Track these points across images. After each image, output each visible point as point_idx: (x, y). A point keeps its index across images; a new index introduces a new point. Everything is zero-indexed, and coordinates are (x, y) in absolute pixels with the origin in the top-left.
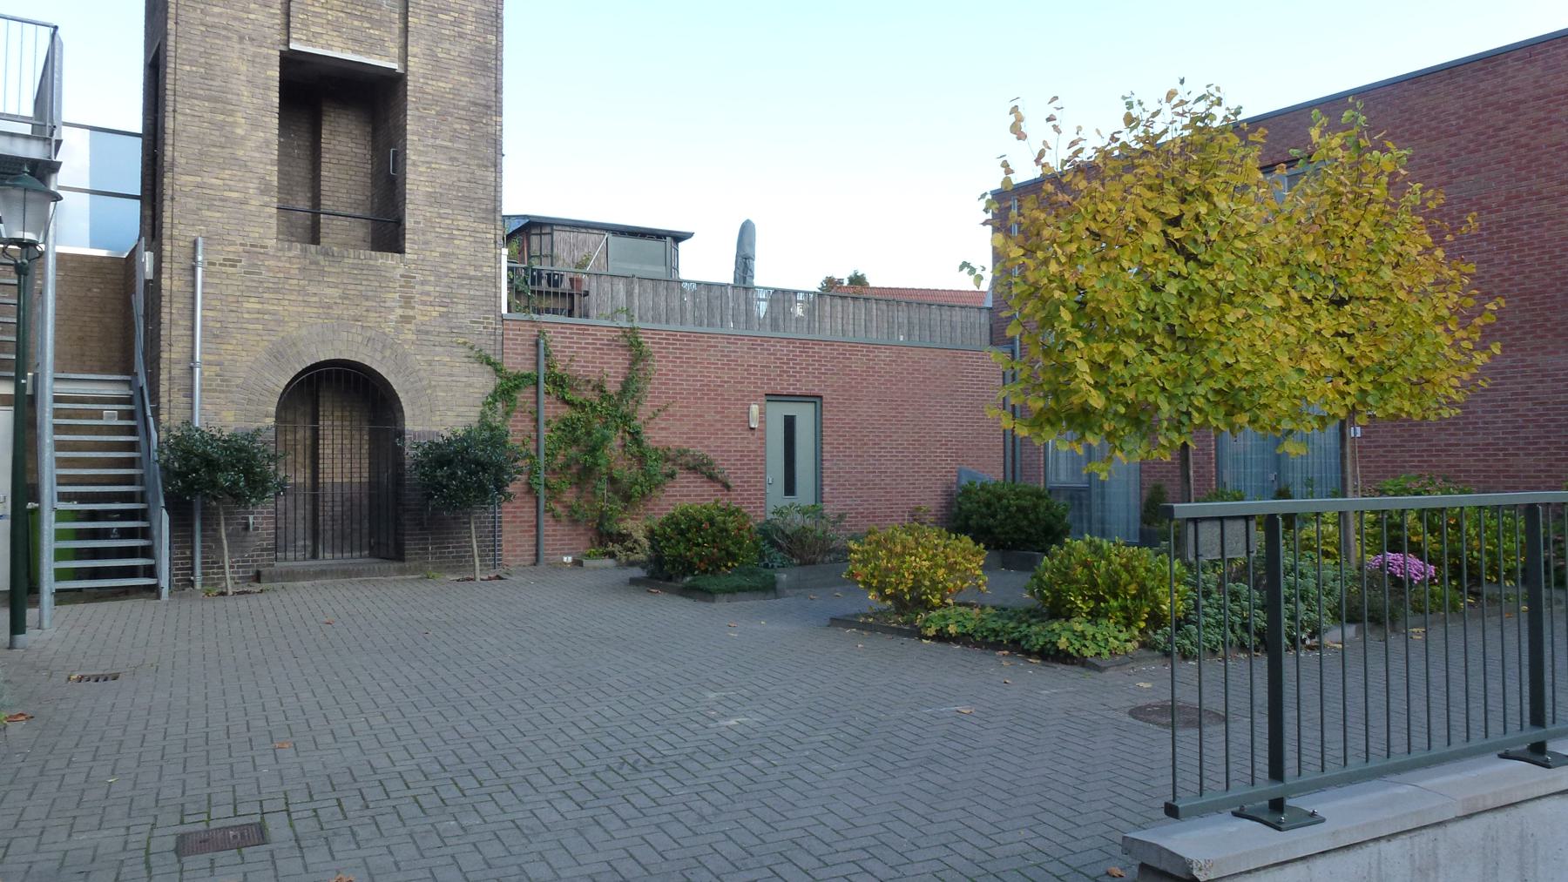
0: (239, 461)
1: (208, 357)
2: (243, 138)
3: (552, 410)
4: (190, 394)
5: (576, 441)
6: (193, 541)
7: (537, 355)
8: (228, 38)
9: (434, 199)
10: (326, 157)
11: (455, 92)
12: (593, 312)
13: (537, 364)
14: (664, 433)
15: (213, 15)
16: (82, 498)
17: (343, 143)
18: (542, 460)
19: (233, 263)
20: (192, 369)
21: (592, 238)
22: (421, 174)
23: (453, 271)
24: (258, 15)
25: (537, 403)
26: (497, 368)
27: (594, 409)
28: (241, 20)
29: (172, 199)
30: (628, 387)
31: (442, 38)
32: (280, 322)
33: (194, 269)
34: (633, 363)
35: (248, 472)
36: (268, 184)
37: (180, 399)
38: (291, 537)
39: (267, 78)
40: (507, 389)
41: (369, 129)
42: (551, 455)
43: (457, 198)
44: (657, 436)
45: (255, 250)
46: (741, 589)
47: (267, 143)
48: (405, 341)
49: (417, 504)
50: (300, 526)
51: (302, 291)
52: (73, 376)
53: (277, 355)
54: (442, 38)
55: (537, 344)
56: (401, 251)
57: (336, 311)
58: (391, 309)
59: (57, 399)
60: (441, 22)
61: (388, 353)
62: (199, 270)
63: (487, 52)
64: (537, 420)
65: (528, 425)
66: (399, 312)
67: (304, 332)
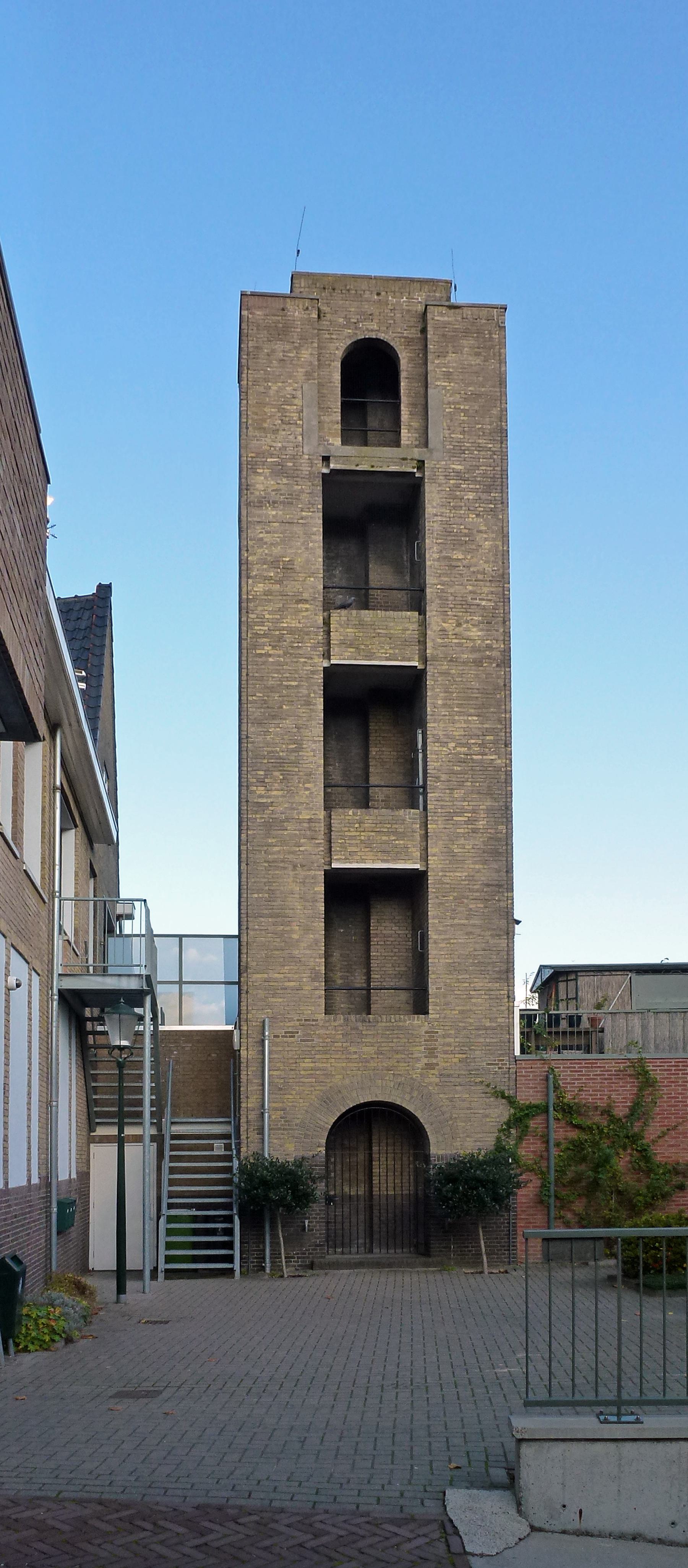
0: (287, 1181)
1: (274, 1105)
2: (298, 941)
3: (560, 1133)
4: (261, 1131)
5: (584, 1159)
6: (264, 1239)
7: (547, 1088)
8: (285, 868)
9: (452, 968)
10: (374, 941)
11: (471, 878)
12: (608, 1046)
13: (547, 1095)
14: (673, 1150)
15: (273, 853)
16: (199, 1207)
17: (387, 928)
18: (552, 1177)
19: (292, 1035)
20: (263, 1114)
21: (617, 978)
22: (442, 949)
23: (471, 1024)
24: (307, 847)
25: (547, 1127)
26: (511, 1101)
27: (601, 1132)
28: (294, 853)
29: (247, 992)
30: (637, 1110)
31: (458, 836)
32: (327, 1075)
33: (263, 1041)
34: (641, 1089)
35: (295, 1189)
36: (317, 973)
37: (254, 1136)
38: (354, 1235)
39: (315, 893)
40: (520, 1118)
41: (409, 914)
42: (561, 1171)
43: (473, 964)
44: (664, 1153)
45: (308, 1023)
46: (360, 1265)
47: (316, 942)
48: (430, 1084)
49: (450, 1213)
50: (361, 1228)
51: (345, 1050)
52: (191, 1120)
53: (326, 1101)
54: (458, 836)
55: (547, 1079)
56: (426, 1013)
57: (373, 1064)
58: (418, 1059)
59: (173, 1137)
60: (457, 824)
61: (415, 1094)
62: (267, 1042)
63: (499, 840)
64: (547, 1142)
65: (539, 1146)
66: (425, 1061)
67: (347, 1081)
